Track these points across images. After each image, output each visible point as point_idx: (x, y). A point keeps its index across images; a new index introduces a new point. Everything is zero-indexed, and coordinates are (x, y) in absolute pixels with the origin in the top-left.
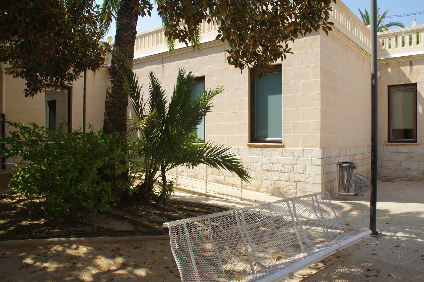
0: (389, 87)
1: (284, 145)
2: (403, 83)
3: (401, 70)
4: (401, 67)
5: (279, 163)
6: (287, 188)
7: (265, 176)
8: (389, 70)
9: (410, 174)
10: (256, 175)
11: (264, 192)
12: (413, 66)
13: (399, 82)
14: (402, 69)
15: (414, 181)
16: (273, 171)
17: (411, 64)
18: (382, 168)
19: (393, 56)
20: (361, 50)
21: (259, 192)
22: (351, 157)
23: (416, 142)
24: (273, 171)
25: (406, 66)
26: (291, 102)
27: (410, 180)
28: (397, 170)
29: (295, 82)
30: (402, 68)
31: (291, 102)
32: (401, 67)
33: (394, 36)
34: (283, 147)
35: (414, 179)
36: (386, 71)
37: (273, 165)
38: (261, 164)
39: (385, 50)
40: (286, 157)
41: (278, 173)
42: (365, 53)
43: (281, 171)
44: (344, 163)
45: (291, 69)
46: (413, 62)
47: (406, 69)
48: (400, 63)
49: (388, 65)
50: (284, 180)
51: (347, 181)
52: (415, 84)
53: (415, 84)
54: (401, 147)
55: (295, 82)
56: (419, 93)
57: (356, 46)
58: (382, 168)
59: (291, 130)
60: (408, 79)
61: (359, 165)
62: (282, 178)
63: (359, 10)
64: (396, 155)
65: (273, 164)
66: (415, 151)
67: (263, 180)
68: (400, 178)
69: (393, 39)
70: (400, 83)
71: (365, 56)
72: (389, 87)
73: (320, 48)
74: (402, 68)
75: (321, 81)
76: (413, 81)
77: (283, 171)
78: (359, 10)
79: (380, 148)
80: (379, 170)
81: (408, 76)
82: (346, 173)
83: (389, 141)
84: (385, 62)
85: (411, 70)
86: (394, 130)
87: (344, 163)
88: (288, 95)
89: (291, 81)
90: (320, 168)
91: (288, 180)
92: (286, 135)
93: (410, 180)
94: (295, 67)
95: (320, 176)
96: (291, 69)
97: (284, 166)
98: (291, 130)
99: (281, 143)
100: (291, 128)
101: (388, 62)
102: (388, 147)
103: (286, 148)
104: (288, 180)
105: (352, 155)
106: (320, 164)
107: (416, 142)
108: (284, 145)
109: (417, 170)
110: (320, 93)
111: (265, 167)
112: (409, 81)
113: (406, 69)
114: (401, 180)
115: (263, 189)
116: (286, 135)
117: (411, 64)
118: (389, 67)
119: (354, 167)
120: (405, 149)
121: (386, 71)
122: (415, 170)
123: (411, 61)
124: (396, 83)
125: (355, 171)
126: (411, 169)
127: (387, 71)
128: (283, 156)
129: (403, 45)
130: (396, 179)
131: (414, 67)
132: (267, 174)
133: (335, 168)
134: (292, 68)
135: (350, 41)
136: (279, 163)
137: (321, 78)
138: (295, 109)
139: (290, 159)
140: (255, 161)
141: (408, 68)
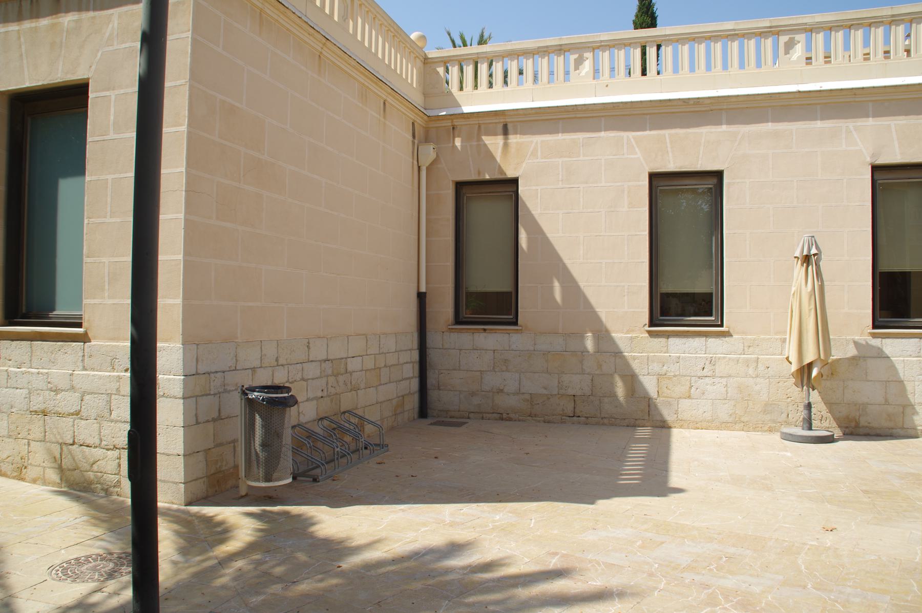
0: (460, 186)
1: (86, 334)
2: (487, 177)
3: (485, 145)
4: (483, 137)
5: (72, 388)
6: (95, 467)
7: (37, 433)
8: (458, 142)
9: (508, 402)
10: (13, 427)
11: (34, 481)
12: (511, 137)
13: (479, 173)
14: (487, 142)
15: (510, 419)
16: (59, 414)
17: (506, 132)
18: (439, 389)
19: (467, 109)
20: (375, 80)
21: (23, 479)
22: (328, 364)
23: (515, 323)
24: (59, 414)
25: (495, 134)
26: (109, 199)
27: (503, 417)
28: (473, 394)
29: (121, 136)
30: (488, 140)
31: (109, 199)
32: (483, 137)
33: (472, 61)
34: (84, 338)
35: (512, 416)
36: (451, 145)
37: (59, 396)
38: (25, 391)
39: (450, 94)
40: (93, 369)
41: (70, 420)
42: (390, 90)
43: (77, 413)
44: (253, 389)
45: (113, 98)
46: (510, 127)
47: (494, 143)
48: (482, 126)
49: (456, 132)
50: (88, 442)
51: (264, 445)
52: (515, 182)
53: (515, 182)
54: (483, 335)
55: (121, 136)
56: (524, 202)
57: (354, 63)
58: (439, 389)
59: (107, 287)
60: (500, 166)
61: (362, 386)
62: (81, 437)
63: (449, 34)
64: (472, 354)
65: (57, 391)
66: (514, 347)
67: (32, 444)
68: (480, 415)
69: (469, 70)
70: (481, 178)
71: (390, 100)
72: (460, 186)
73: (189, 34)
74: (488, 140)
75: (189, 133)
76: (510, 174)
77: (84, 414)
78: (449, 34)
79: (433, 339)
80: (433, 395)
81: (498, 159)
82: (257, 417)
83: (459, 320)
84: (448, 124)
85: (506, 145)
86: (470, 295)
87: (253, 389)
88: (102, 177)
89: (112, 136)
90: (182, 407)
91: (97, 442)
92: (92, 301)
93: (502, 419)
94: (122, 91)
95: (181, 432)
96: (113, 98)
97: (87, 397)
98: (107, 287)
99: (79, 325)
100: (106, 279)
101: (457, 122)
102: (454, 336)
103: (93, 343)
104: (97, 442)
105: (332, 360)
106: (181, 395)
107: (515, 323)
108: (86, 334)
109: (518, 393)
110: (184, 170)
111: (37, 403)
112: (501, 171)
113: (494, 143)
114: (483, 418)
115: (31, 472)
116: (92, 301)
117: (506, 132)
118: (459, 136)
119: (291, 402)
120: (491, 340)
121: (451, 145)
122: (514, 394)
123: (506, 123)
124: (473, 177)
125: (292, 415)
126: (505, 390)
127: (454, 146)
128: (84, 369)
129: (491, 85)
130: (471, 415)
131: (513, 139)
132: (42, 422)
133: (235, 405)
134: (117, 92)
135: (328, 43)
136: (72, 388)
137: (189, 125)
138: (118, 220)
139: (100, 377)
140: (12, 382)
141: (500, 140)
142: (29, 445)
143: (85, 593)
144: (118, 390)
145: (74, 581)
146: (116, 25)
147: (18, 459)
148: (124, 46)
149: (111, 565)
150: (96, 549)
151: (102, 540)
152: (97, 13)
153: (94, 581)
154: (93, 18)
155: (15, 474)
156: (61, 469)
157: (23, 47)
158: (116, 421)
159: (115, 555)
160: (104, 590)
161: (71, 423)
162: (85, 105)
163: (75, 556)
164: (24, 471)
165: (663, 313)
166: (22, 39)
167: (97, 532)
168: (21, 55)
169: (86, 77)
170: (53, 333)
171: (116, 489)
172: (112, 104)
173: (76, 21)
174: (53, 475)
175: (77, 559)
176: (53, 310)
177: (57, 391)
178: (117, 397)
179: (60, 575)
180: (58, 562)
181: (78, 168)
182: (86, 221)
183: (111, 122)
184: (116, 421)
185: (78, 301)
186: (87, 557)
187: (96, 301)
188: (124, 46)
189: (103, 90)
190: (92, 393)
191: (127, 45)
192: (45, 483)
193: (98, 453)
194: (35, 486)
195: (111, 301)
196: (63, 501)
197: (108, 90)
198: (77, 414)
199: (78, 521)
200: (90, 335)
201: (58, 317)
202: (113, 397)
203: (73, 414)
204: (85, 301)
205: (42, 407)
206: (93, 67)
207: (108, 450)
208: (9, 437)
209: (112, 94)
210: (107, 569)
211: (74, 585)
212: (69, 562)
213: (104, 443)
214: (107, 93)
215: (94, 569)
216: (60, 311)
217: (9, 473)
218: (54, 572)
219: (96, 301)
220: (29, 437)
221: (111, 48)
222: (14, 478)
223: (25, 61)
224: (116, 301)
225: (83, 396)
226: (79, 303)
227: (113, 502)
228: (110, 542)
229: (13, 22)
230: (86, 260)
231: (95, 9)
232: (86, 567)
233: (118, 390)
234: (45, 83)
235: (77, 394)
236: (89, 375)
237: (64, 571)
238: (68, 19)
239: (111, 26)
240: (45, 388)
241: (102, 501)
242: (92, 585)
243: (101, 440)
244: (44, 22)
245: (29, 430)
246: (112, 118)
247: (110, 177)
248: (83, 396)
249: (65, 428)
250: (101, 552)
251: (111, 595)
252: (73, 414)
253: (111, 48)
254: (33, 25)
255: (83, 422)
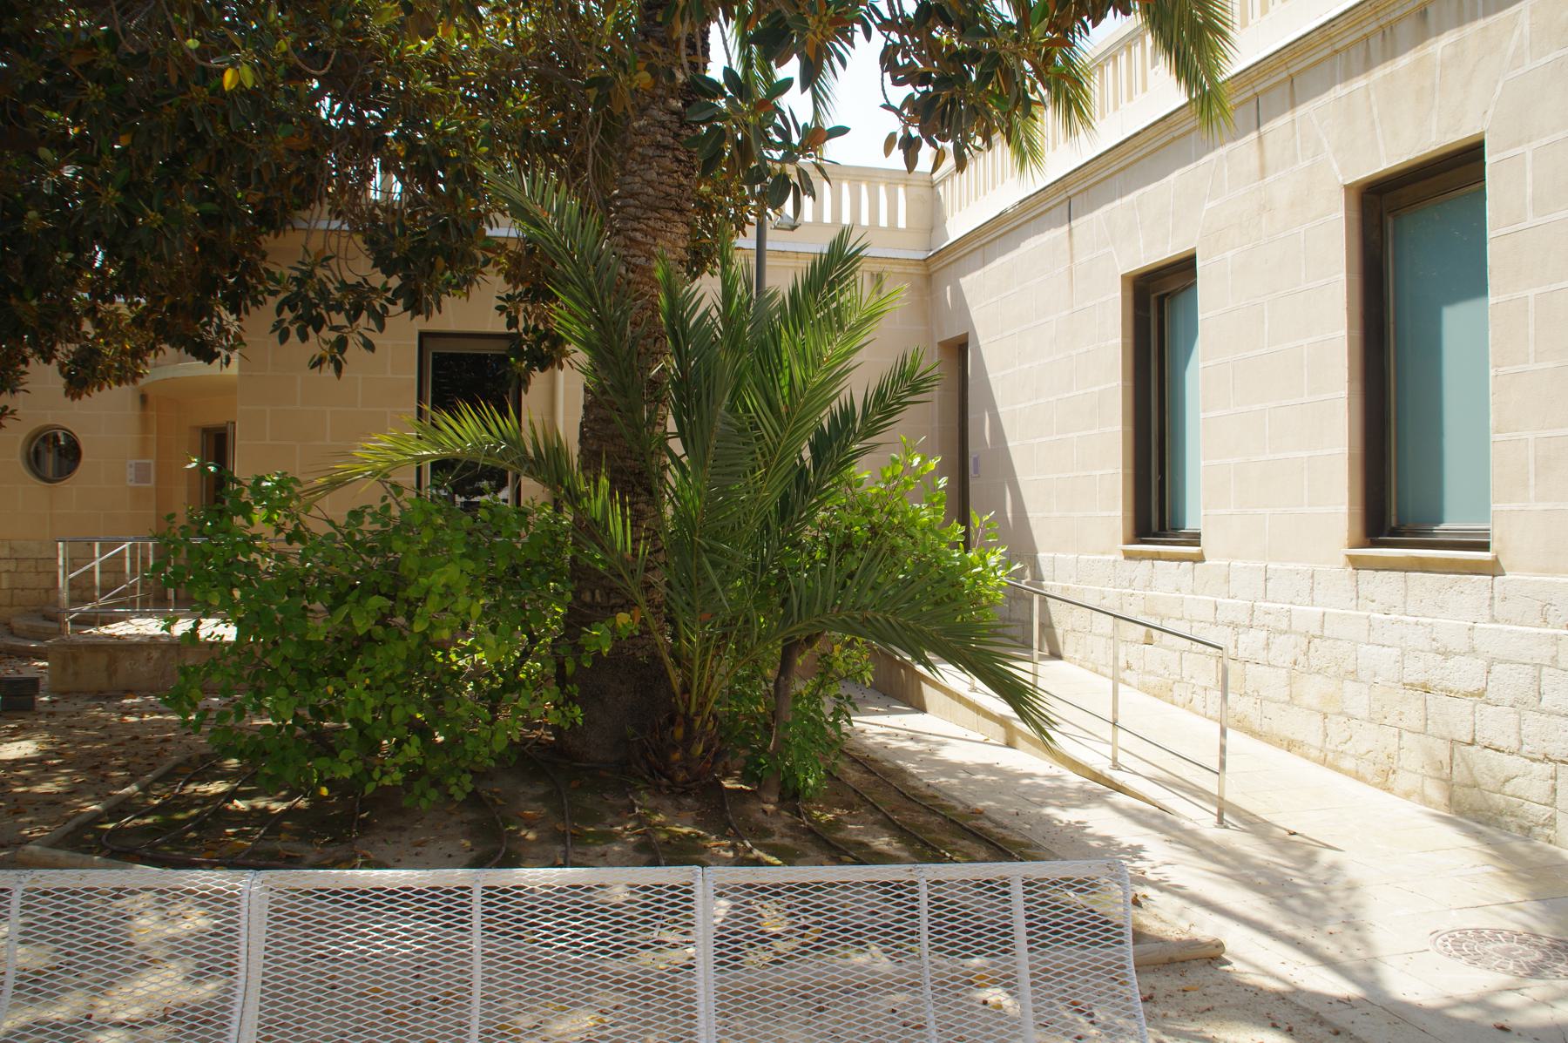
1: (1496, 561)
6: (1508, 789)
7: (1413, 719)
11: (1407, 795)
16: (1450, 693)
21: (1389, 790)
24: (1450, 693)
31: (1531, 331)
34: (1493, 569)
37: (1450, 663)
38: (1397, 651)
41: (1467, 703)
43: (1481, 693)
45: (1529, 156)
50: (1497, 744)
59: (1532, 482)
65: (1446, 654)
67: (1406, 735)
77: (1492, 694)
89: (1531, 220)
91: (1514, 745)
92: (1506, 507)
94: (1545, 141)
96: (1529, 156)
97: (1497, 668)
98: (1532, 482)
99: (1485, 547)
100: (1532, 468)
103: (1509, 576)
104: (1514, 745)
108: (1496, 561)
111: (1414, 674)
115: (1403, 781)
116: (1506, 507)
128: (1494, 620)
132: (1420, 703)
134: (1535, 144)
136: (1473, 650)
138: (1551, 365)
142: (1400, 736)
143: (1492, 986)
144: (1554, 659)
145: (1473, 963)
146: (1527, 29)
147: (1383, 757)
148: (1543, 61)
149: (1538, 955)
150: (1511, 921)
151: (1520, 910)
152: (1490, 19)
153: (1507, 973)
154: (1485, 29)
155: (1378, 780)
156: (1448, 784)
157: (1375, 110)
158: (1551, 713)
159: (1545, 941)
160: (1525, 991)
161: (1469, 710)
162: (1481, 178)
163: (1474, 926)
164: (1392, 777)
165: (440, 360)
166: (1373, 97)
167: (1513, 896)
168: (1373, 123)
169: (1478, 131)
170: (1441, 560)
171: (1547, 831)
172: (1528, 167)
173: (1456, 44)
174: (1435, 792)
175: (1476, 930)
176: (1440, 521)
177: (1446, 654)
178: (1552, 671)
179: (1450, 947)
180: (1446, 927)
181: (1474, 284)
182: (1492, 372)
183: (1528, 199)
184: (1551, 713)
185: (1482, 506)
186: (1495, 933)
187: (1515, 506)
188: (1543, 61)
189: (1510, 147)
190: (1507, 662)
191: (1550, 57)
192: (1425, 800)
193: (1513, 764)
194: (1408, 803)
195: (1541, 506)
196: (1452, 837)
197: (1520, 143)
198: (1481, 695)
199: (1476, 870)
200: (1503, 564)
201: (1448, 532)
202: (1545, 670)
203: (1472, 694)
204: (1494, 507)
205: (1422, 678)
206: (1490, 112)
207: (1533, 760)
208: (1371, 721)
209: (1527, 150)
210: (1529, 959)
211: (1472, 969)
212: (1463, 932)
213: (1526, 748)
214: (1519, 150)
215: (1507, 953)
216: (1453, 523)
217: (1369, 777)
218: (1439, 941)
219: (1515, 506)
220: (1401, 724)
221: (1520, 71)
222: (1376, 785)
223: (1379, 131)
224: (1549, 506)
225: (1490, 665)
226: (1484, 510)
227: (1538, 850)
228: (1535, 916)
229: (1358, 75)
230: (1494, 437)
231: (1485, 15)
232: (1492, 946)
233: (1554, 659)
234: (1412, 156)
235: (1480, 662)
236: (1501, 631)
237: (1457, 944)
238: (1440, 46)
239: (1517, 33)
240: (1427, 648)
241: (1519, 846)
242: (1501, 978)
243: (1521, 743)
244: (1404, 61)
245: (1402, 713)
246: (1529, 190)
247: (1531, 293)
248: (1490, 665)
249: (1459, 717)
250: (1519, 929)
251: (1536, 1003)
252: (1472, 694)
253: (1520, 71)
254: (1388, 70)
255: (1490, 709)
